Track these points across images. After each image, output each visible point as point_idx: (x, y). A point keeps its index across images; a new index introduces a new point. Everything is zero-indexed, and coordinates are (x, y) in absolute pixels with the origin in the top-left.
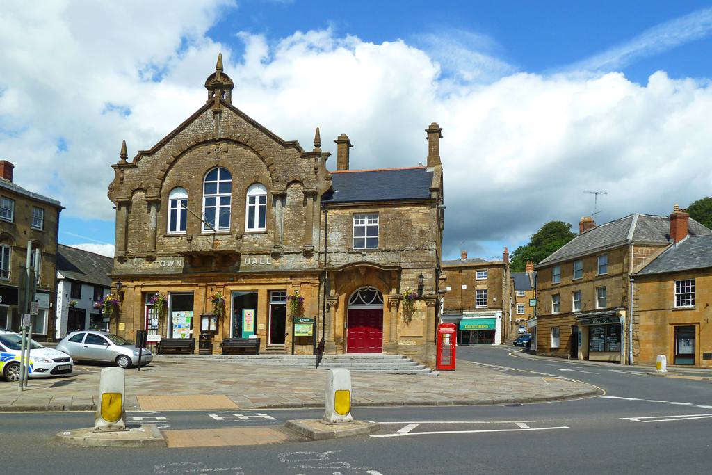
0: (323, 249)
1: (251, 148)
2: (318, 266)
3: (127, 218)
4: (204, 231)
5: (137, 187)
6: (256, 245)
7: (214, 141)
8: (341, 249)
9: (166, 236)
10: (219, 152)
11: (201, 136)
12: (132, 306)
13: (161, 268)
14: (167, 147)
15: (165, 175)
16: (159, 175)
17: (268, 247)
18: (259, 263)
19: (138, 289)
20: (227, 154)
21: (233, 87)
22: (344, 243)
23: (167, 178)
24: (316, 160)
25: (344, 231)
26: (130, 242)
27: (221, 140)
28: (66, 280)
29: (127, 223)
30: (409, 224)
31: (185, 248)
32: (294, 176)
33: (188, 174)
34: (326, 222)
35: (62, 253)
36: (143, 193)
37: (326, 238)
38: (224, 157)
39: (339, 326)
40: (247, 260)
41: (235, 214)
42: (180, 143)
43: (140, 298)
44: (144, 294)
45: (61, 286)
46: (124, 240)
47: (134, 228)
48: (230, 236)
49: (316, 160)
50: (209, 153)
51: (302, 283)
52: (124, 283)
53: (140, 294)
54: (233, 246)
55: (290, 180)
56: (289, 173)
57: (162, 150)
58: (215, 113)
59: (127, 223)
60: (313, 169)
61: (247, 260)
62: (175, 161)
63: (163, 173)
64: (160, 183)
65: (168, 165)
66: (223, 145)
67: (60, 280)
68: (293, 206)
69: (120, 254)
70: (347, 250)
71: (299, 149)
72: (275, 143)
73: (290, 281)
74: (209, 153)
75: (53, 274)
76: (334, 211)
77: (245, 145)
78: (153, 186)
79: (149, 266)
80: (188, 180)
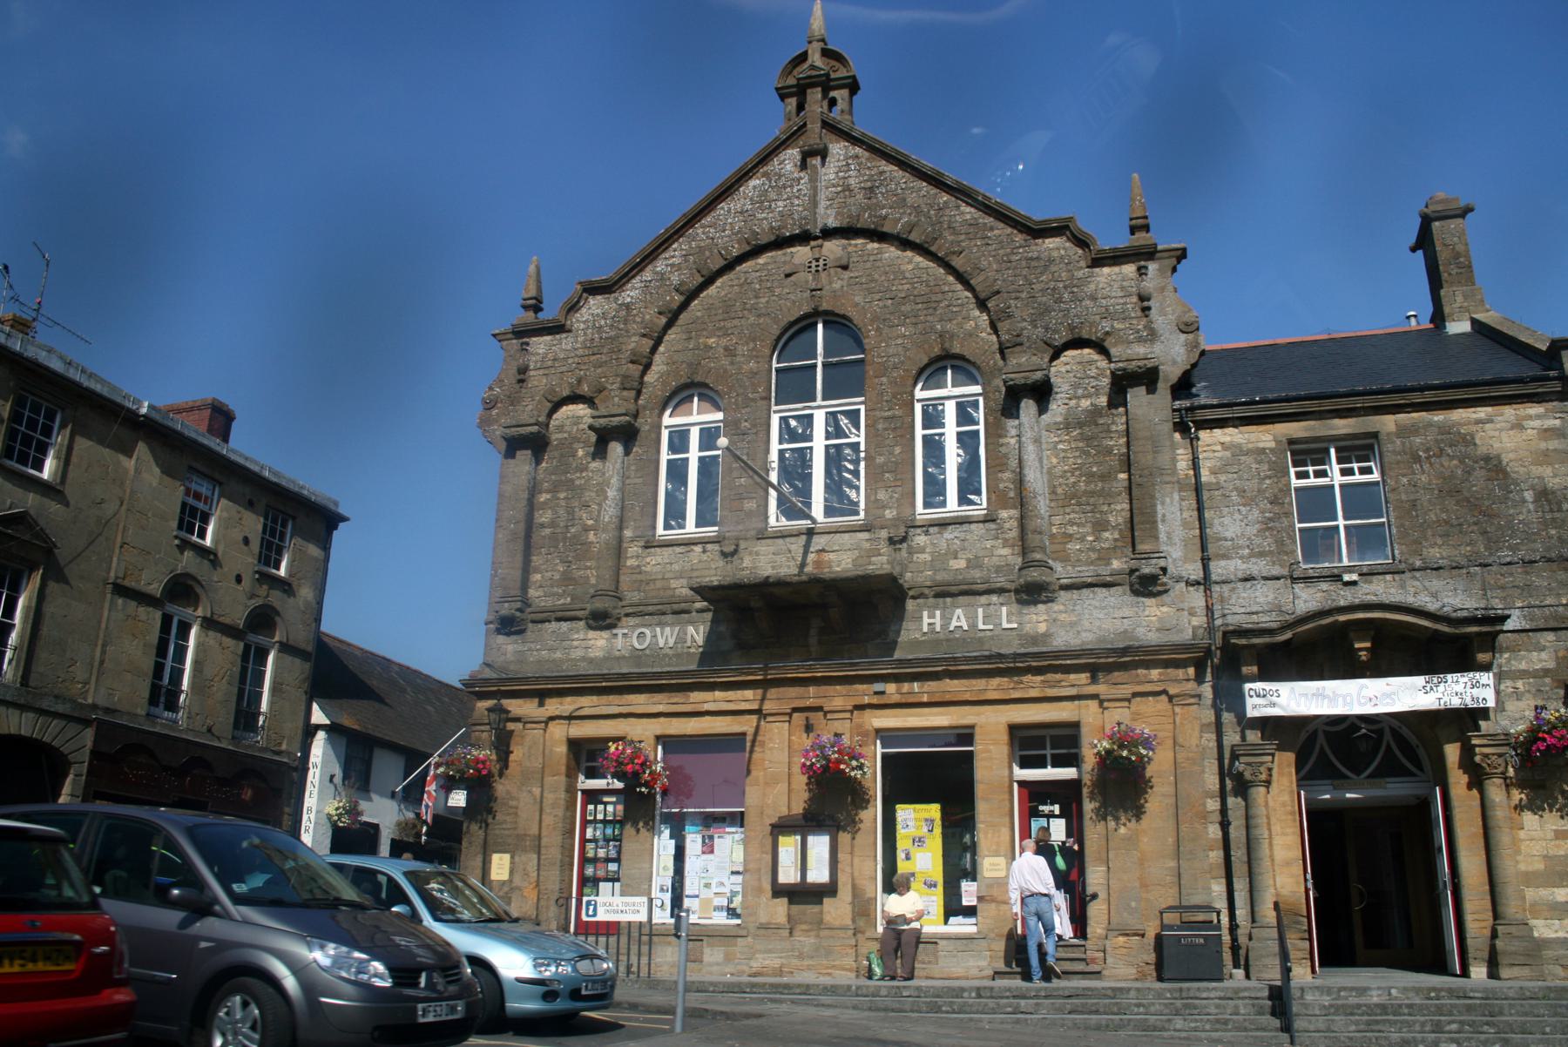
0: (1194, 571)
1: (922, 249)
2: (1191, 637)
3: (534, 490)
4: (775, 519)
5: (566, 393)
6: (960, 564)
7: (804, 238)
8: (1259, 567)
9: (651, 544)
10: (818, 266)
11: (766, 223)
12: (537, 791)
13: (637, 656)
14: (660, 265)
15: (654, 350)
16: (634, 352)
17: (998, 569)
18: (973, 626)
19: (559, 732)
20: (846, 275)
21: (859, 88)
22: (1268, 544)
23: (657, 358)
24: (1141, 271)
25: (1265, 505)
26: (537, 570)
27: (828, 233)
28: (332, 729)
29: (531, 506)
30: (1495, 467)
31: (715, 572)
32: (1071, 328)
33: (724, 342)
34: (1197, 475)
35: (326, 639)
36: (581, 410)
37: (1202, 528)
38: (837, 282)
39: (1288, 864)
40: (932, 616)
41: (880, 460)
42: (701, 250)
43: (564, 761)
44: (574, 745)
45: (319, 748)
46: (519, 558)
47: (553, 524)
48: (865, 535)
49: (1141, 271)
50: (788, 276)
51: (1135, 695)
52: (515, 706)
53: (562, 749)
54: (880, 563)
55: (1059, 340)
56: (1054, 318)
57: (647, 275)
58: (806, 155)
59: (531, 506)
60: (1135, 299)
61: (932, 616)
62: (684, 306)
63: (647, 344)
64: (637, 374)
65: (664, 320)
66: (833, 248)
67: (318, 727)
68: (1080, 425)
69: (506, 609)
70: (1285, 572)
71: (1081, 242)
72: (1002, 230)
73: (1092, 689)
74: (788, 276)
75: (302, 714)
76: (1219, 434)
77: (905, 244)
78: (614, 386)
79: (599, 643)
80: (725, 362)
